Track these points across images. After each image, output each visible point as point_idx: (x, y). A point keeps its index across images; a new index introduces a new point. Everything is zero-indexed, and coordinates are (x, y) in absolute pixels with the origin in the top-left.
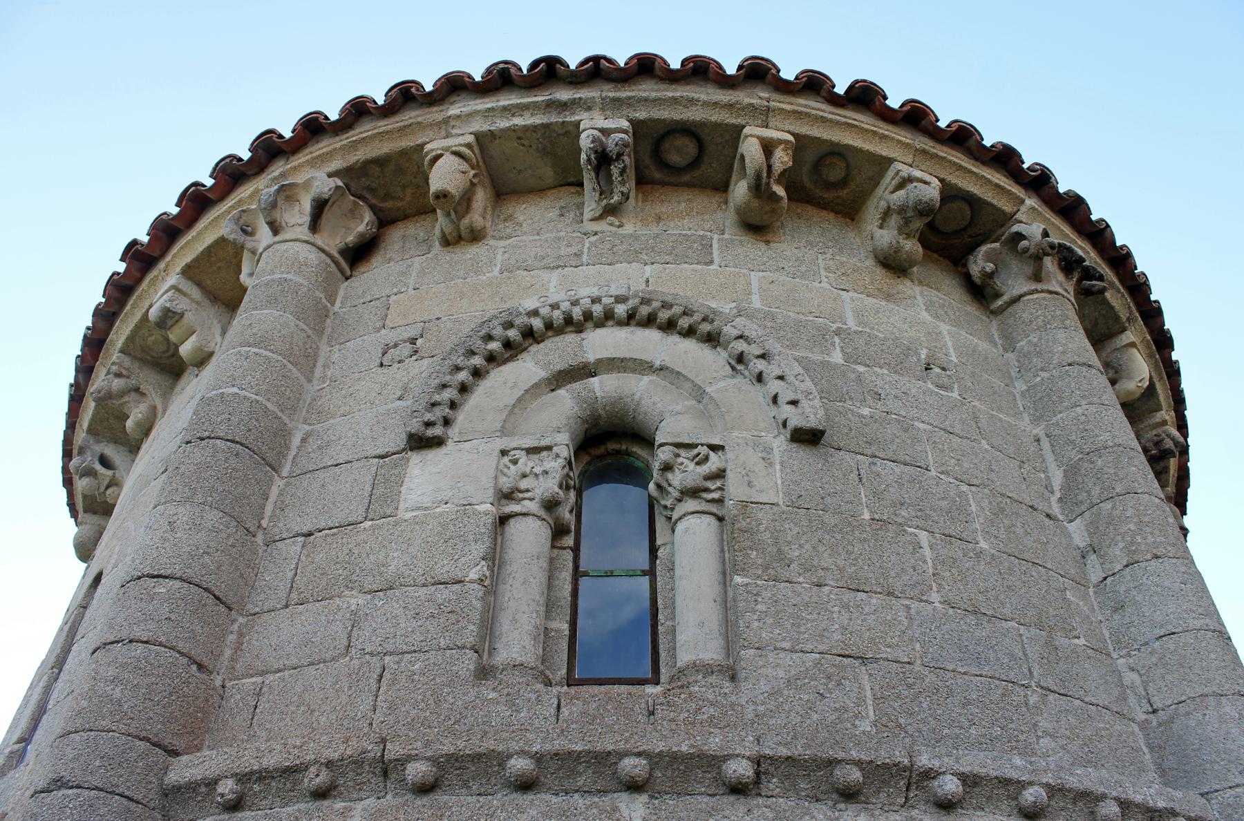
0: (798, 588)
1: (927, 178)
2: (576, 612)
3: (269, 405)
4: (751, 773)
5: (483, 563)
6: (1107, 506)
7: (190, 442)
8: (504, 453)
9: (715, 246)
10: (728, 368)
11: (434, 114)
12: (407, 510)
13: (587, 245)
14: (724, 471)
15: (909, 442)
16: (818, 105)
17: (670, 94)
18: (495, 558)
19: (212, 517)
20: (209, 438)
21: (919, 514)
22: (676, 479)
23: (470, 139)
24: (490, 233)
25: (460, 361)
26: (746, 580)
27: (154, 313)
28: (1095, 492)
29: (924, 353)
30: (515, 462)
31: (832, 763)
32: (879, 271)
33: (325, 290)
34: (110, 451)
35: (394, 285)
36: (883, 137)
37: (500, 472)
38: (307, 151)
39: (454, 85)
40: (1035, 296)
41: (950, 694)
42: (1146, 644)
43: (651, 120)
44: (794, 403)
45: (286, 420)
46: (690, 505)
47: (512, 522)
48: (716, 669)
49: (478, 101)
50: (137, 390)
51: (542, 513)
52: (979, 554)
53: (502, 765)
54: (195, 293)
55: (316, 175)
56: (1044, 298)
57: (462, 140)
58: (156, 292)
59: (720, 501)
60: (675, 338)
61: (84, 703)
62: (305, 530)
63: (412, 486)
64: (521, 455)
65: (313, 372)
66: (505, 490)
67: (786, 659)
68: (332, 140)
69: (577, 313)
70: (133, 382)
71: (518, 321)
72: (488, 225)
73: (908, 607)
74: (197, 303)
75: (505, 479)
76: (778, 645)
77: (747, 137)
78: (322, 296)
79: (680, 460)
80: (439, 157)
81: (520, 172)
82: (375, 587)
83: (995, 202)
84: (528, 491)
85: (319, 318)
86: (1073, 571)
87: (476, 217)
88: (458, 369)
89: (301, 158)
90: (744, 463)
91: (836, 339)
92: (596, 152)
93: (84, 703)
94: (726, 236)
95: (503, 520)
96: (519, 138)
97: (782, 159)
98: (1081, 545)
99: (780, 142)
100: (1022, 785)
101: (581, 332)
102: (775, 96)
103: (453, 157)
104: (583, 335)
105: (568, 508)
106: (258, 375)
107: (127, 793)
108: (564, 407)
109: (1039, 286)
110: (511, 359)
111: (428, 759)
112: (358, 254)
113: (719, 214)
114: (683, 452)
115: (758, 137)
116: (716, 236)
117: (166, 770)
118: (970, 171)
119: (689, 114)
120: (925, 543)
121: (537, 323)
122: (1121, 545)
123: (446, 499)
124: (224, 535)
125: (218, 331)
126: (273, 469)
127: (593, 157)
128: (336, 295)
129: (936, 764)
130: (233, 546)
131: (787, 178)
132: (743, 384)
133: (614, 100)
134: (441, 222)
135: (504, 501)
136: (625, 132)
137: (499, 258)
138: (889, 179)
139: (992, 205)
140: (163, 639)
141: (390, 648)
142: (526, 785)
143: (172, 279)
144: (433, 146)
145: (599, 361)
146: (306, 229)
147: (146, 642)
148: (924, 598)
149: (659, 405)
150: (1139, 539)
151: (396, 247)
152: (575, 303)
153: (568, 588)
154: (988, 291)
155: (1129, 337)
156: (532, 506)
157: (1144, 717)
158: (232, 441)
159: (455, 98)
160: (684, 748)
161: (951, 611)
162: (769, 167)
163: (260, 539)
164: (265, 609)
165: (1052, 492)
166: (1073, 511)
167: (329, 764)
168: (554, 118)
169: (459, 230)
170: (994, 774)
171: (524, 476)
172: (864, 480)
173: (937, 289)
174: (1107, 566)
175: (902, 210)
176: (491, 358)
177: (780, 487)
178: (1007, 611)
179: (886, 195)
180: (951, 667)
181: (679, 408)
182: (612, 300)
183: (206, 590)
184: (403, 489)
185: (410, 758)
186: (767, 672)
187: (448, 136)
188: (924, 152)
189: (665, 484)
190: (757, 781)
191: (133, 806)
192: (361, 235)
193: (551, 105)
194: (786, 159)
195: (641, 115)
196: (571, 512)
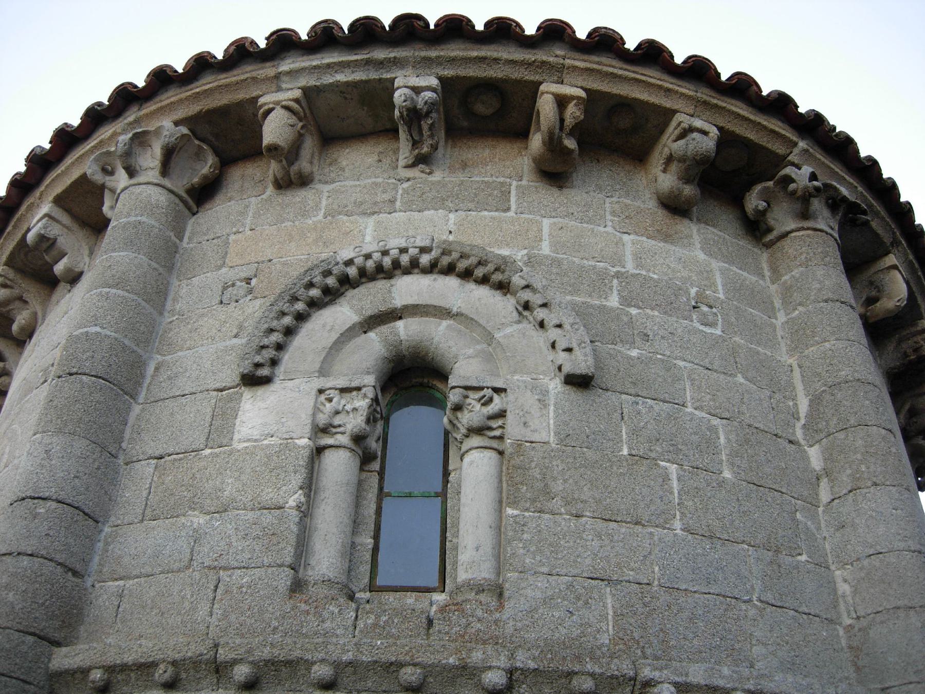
1: (706, 126)
2: (379, 529)
3: (127, 342)
4: (504, 681)
5: (300, 492)
6: (841, 435)
8: (321, 391)
9: (513, 193)
10: (515, 314)
11: (268, 70)
12: (240, 441)
13: (400, 192)
14: (505, 411)
15: (669, 380)
17: (475, 54)
18: (310, 486)
19: (80, 445)
20: (76, 374)
21: (671, 448)
24: (317, 178)
25: (286, 307)
26: (516, 512)
27: (30, 237)
29: (693, 291)
30: (330, 400)
31: (570, 674)
32: (661, 213)
33: (174, 229)
35: (234, 224)
37: (316, 410)
39: (283, 42)
40: (801, 233)
41: (680, 610)
42: (858, 559)
43: (458, 77)
44: (569, 350)
46: (476, 441)
48: (486, 588)
49: (305, 58)
50: (20, 299)
52: (722, 483)
53: (309, 670)
54: (65, 219)
55: (165, 123)
56: (808, 236)
59: (501, 438)
60: (471, 286)
62: (157, 454)
63: (244, 419)
64: (332, 393)
65: (164, 306)
66: (321, 425)
67: (541, 582)
68: (178, 91)
70: (16, 292)
71: (336, 270)
72: (315, 169)
74: (67, 228)
77: (543, 93)
78: (172, 234)
79: (468, 401)
81: (343, 119)
82: (212, 509)
83: (769, 146)
84: (340, 426)
85: (168, 257)
86: (806, 493)
87: (303, 164)
88: (284, 314)
90: (522, 405)
91: (615, 281)
94: (524, 182)
95: (320, 451)
97: (573, 112)
98: (818, 468)
99: (572, 98)
103: (283, 111)
104: (393, 281)
105: (375, 438)
106: (117, 314)
107: (22, 677)
108: (373, 347)
109: (806, 224)
110: (331, 302)
111: (251, 663)
112: (203, 194)
113: (519, 159)
115: (553, 94)
116: (514, 183)
120: (674, 477)
121: (352, 271)
122: (849, 472)
123: (272, 432)
124: (91, 460)
125: (87, 252)
126: (131, 397)
128: (184, 231)
129: (656, 675)
130: (98, 468)
131: (578, 131)
132: (528, 328)
135: (320, 435)
137: (324, 202)
138: (672, 130)
139: (767, 149)
140: (44, 552)
141: (223, 563)
144: (267, 99)
147: (31, 555)
148: (668, 526)
149: (454, 349)
150: (863, 468)
151: (237, 186)
152: (385, 253)
153: (373, 506)
155: (891, 260)
156: (344, 439)
157: (849, 622)
158: (95, 376)
160: (451, 660)
161: (690, 537)
162: (562, 120)
163: (121, 461)
164: (125, 522)
165: (798, 419)
167: (174, 663)
168: (373, 75)
169: (289, 175)
171: (337, 413)
172: (626, 418)
173: (713, 226)
174: (836, 489)
175: (682, 159)
176: (314, 305)
177: (552, 426)
178: (739, 535)
179: (669, 144)
180: (684, 587)
182: (417, 250)
183: (77, 508)
184: (238, 422)
185: (235, 662)
186: (527, 592)
187: (280, 89)
188: (705, 103)
189: (455, 422)
191: (27, 687)
192: (205, 177)
194: (578, 114)
195: (449, 72)
196: (377, 441)
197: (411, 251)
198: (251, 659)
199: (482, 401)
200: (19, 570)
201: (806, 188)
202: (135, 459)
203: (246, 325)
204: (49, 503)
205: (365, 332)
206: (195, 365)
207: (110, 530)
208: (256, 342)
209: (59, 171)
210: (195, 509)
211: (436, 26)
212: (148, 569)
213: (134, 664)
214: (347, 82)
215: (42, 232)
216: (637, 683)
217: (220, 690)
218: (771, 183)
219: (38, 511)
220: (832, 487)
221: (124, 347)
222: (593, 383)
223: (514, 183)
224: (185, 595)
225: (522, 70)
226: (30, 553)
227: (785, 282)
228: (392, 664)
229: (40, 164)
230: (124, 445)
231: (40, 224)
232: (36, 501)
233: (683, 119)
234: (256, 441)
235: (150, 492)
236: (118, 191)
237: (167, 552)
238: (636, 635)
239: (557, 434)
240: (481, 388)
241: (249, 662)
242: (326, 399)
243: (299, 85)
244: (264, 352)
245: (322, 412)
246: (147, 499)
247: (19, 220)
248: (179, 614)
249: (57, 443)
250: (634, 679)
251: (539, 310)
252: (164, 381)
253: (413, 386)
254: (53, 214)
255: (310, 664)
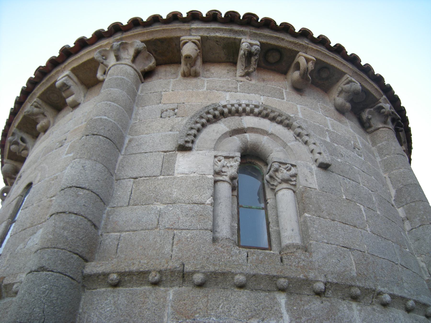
0: (327, 220)
3: (118, 126)
4: (324, 288)
5: (212, 198)
6: (413, 204)
7: (88, 135)
8: (215, 157)
9: (284, 93)
10: (294, 137)
11: (186, 26)
12: (178, 173)
13: (239, 85)
14: (297, 174)
16: (324, 49)
17: (275, 35)
19: (99, 167)
20: (97, 135)
22: (280, 175)
23: (199, 38)
24: (201, 75)
25: (198, 120)
26: (310, 216)
27: (58, 84)
28: (409, 199)
31: (351, 286)
32: (336, 113)
33: (136, 86)
34: (25, 136)
36: (344, 65)
37: (215, 164)
38: (132, 31)
39: (194, 16)
40: (384, 129)
43: (267, 43)
44: (320, 153)
45: (124, 133)
46: (284, 185)
47: (219, 183)
48: (301, 247)
49: (203, 24)
50: (43, 114)
51: (229, 181)
53: (233, 278)
54: (75, 79)
57: (195, 38)
58: (59, 76)
59: (295, 185)
60: (274, 124)
61: (51, 236)
62: (134, 176)
64: (222, 158)
66: (217, 171)
68: (142, 29)
69: (241, 109)
70: (42, 110)
71: (219, 108)
73: (361, 232)
74: (76, 83)
75: (216, 167)
76: (323, 241)
77: (300, 56)
78: (135, 87)
79: (281, 168)
80: (186, 43)
82: (168, 202)
83: (374, 94)
84: (225, 172)
88: (197, 122)
89: (129, 34)
92: (248, 51)
93: (51, 236)
94: (288, 90)
96: (217, 41)
98: (403, 217)
99: (311, 60)
100: (408, 300)
101: (240, 116)
102: (310, 43)
104: (242, 117)
107: (71, 276)
108: (236, 142)
109: (386, 126)
110: (215, 122)
111: (204, 273)
112: (147, 75)
114: (281, 165)
117: (84, 267)
118: (369, 82)
119: (281, 44)
120: (363, 210)
121: (226, 110)
122: (418, 218)
125: (83, 95)
127: (246, 53)
129: (382, 289)
130: (106, 179)
133: (255, 33)
134: (183, 67)
135: (216, 175)
136: (258, 46)
137: (206, 84)
138: (344, 80)
141: (176, 226)
142: (242, 286)
143: (67, 72)
144: (185, 38)
145: (249, 128)
146: (130, 61)
147: (76, 214)
149: (271, 147)
154: (367, 125)
156: (227, 178)
159: (194, 22)
160: (301, 276)
163: (114, 178)
164: (119, 205)
166: (399, 205)
167: (160, 272)
168: (232, 36)
170: (400, 295)
171: (224, 166)
176: (209, 121)
179: (342, 85)
181: (278, 149)
182: (253, 106)
184: (176, 165)
185: (193, 273)
187: (190, 35)
188: (356, 73)
190: (324, 292)
191: (73, 281)
193: (231, 31)
195: (263, 41)
197: (251, 106)
198: (203, 271)
199: (287, 169)
200: (70, 221)
201: (388, 111)
202: (122, 178)
203: (175, 127)
204: (85, 191)
205: (231, 136)
206: (151, 141)
207: (110, 209)
208: (185, 132)
209: (77, 57)
210: (158, 202)
211: (261, 21)
212: (135, 228)
213: (137, 272)
214: (220, 37)
215: (65, 82)
216: (376, 293)
217: (183, 287)
218: (372, 109)
219: (79, 193)
220: (411, 224)
221: (118, 128)
222: (329, 168)
223: (284, 90)
224: (157, 240)
225: (292, 45)
226: (76, 213)
227: (379, 146)
228: (274, 276)
229: (66, 53)
230: (116, 171)
231: (64, 78)
232: (78, 189)
233: (348, 77)
234: (186, 174)
235: (131, 193)
236: (110, 66)
237: (144, 220)
238: (365, 273)
239: (319, 186)
240: (285, 164)
241: (202, 273)
242: (218, 160)
243: (200, 35)
244: (189, 137)
245: (216, 165)
246: (130, 196)
247: (51, 77)
248: (154, 249)
249: (88, 164)
250: (374, 291)
251: (305, 136)
252: (135, 146)
253: (247, 163)
254: (70, 75)
255: (234, 275)
